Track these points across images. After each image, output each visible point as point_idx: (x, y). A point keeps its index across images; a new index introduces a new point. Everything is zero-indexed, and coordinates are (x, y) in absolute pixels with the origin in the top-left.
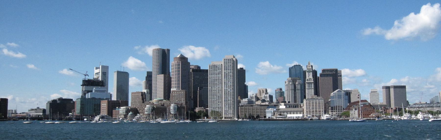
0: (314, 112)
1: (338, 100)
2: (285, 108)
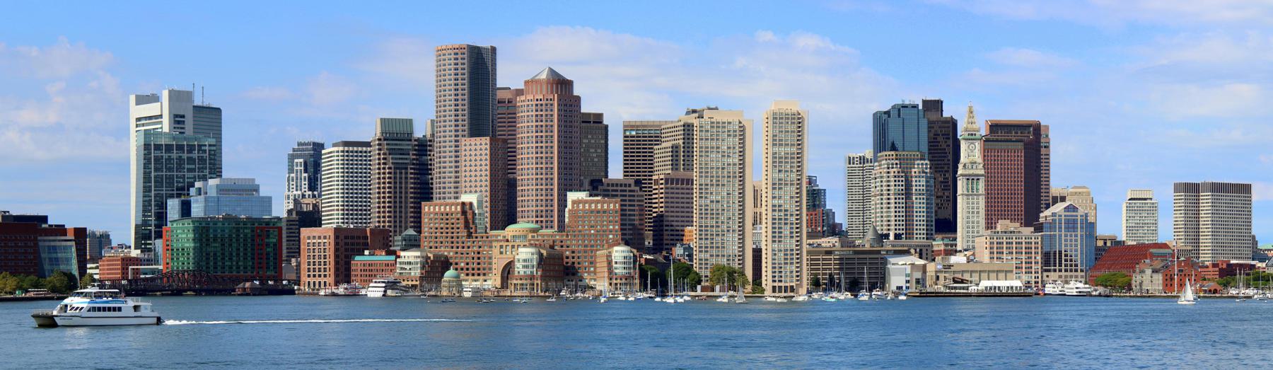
1: (1066, 236)
2: (965, 262)
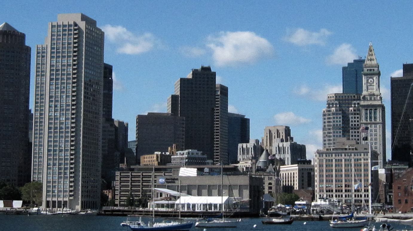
0: (342, 191)
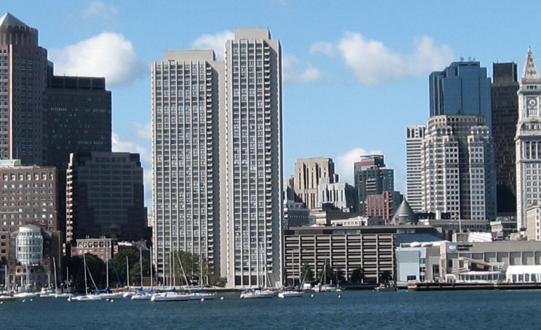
2: (490, 240)
